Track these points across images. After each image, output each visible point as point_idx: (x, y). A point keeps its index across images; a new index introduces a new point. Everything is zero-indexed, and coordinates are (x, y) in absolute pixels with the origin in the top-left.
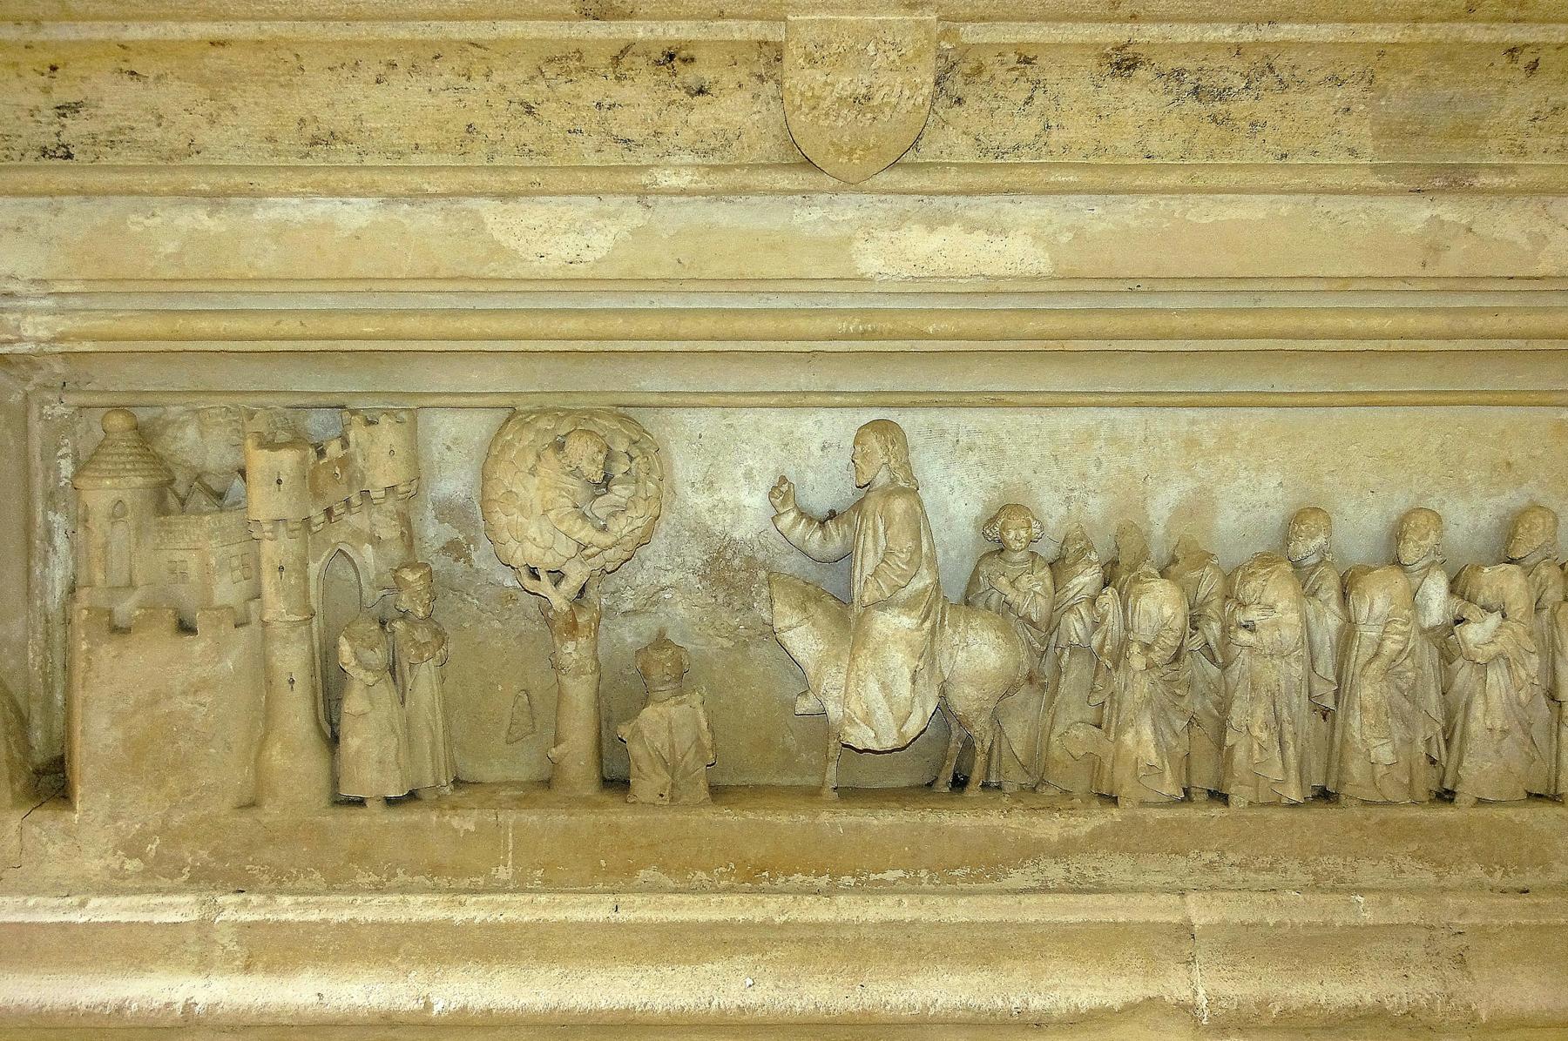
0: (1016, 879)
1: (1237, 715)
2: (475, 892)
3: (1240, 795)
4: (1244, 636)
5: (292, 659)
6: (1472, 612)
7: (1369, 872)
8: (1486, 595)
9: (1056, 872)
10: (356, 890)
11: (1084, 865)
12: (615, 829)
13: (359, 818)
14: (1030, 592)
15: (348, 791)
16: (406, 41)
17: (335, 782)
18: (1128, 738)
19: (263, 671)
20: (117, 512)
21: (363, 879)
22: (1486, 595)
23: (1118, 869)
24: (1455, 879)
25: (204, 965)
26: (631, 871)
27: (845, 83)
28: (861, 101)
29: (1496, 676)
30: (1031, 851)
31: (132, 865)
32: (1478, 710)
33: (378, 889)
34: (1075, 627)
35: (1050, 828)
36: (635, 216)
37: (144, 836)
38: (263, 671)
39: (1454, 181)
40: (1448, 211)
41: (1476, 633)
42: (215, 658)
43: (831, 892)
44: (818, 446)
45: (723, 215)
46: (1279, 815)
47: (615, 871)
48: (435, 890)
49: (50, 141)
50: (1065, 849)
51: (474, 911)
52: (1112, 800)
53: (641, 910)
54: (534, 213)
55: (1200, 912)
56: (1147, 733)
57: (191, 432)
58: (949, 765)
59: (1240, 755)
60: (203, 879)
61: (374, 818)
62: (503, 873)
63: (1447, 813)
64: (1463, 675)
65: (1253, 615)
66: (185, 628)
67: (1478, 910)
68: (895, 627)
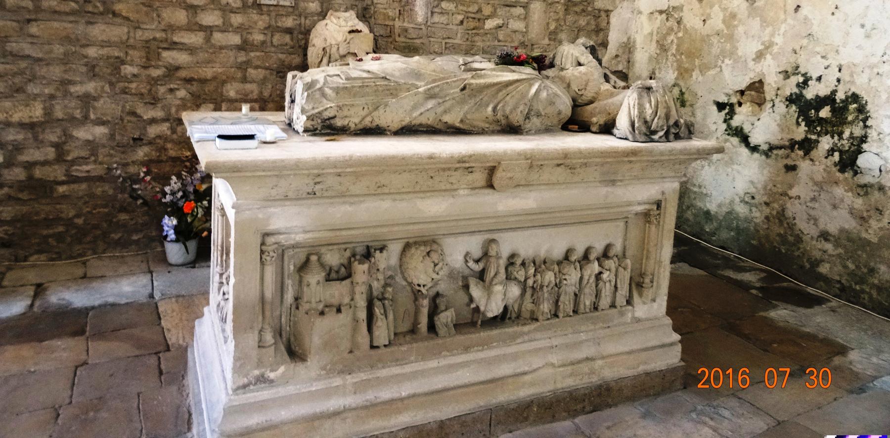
0: (519, 341)
1: (562, 299)
2: (406, 364)
3: (561, 315)
4: (565, 282)
5: (363, 315)
6: (604, 271)
7: (583, 328)
8: (607, 267)
9: (526, 338)
10: (378, 368)
11: (532, 336)
12: (438, 344)
13: (380, 351)
14: (521, 275)
15: (375, 344)
16: (245, 62)
17: (371, 341)
18: (541, 307)
19: (356, 320)
20: (318, 283)
21: (380, 366)
22: (607, 267)
23: (538, 335)
24: (597, 327)
25: (344, 395)
26: (440, 353)
27: (509, 175)
28: (511, 178)
29: (608, 284)
30: (522, 334)
31: (323, 372)
32: (603, 291)
33: (383, 367)
34: (530, 282)
35: (526, 329)
36: (451, 200)
37: (326, 365)
38: (356, 320)
39: (613, 182)
40: (610, 189)
41: (605, 276)
42: (344, 318)
43: (482, 350)
44: (474, 244)
45: (471, 199)
46: (568, 319)
47: (436, 354)
48: (397, 365)
49: (310, 191)
50: (529, 332)
51: (408, 369)
52: (537, 320)
53: (443, 362)
54: (428, 202)
55: (555, 342)
56: (546, 305)
57: (328, 256)
58: (504, 318)
59: (561, 307)
60: (341, 372)
61: (383, 350)
62: (412, 358)
63: (597, 314)
64: (601, 284)
65: (567, 277)
66: (339, 310)
67: (602, 333)
68: (498, 288)
